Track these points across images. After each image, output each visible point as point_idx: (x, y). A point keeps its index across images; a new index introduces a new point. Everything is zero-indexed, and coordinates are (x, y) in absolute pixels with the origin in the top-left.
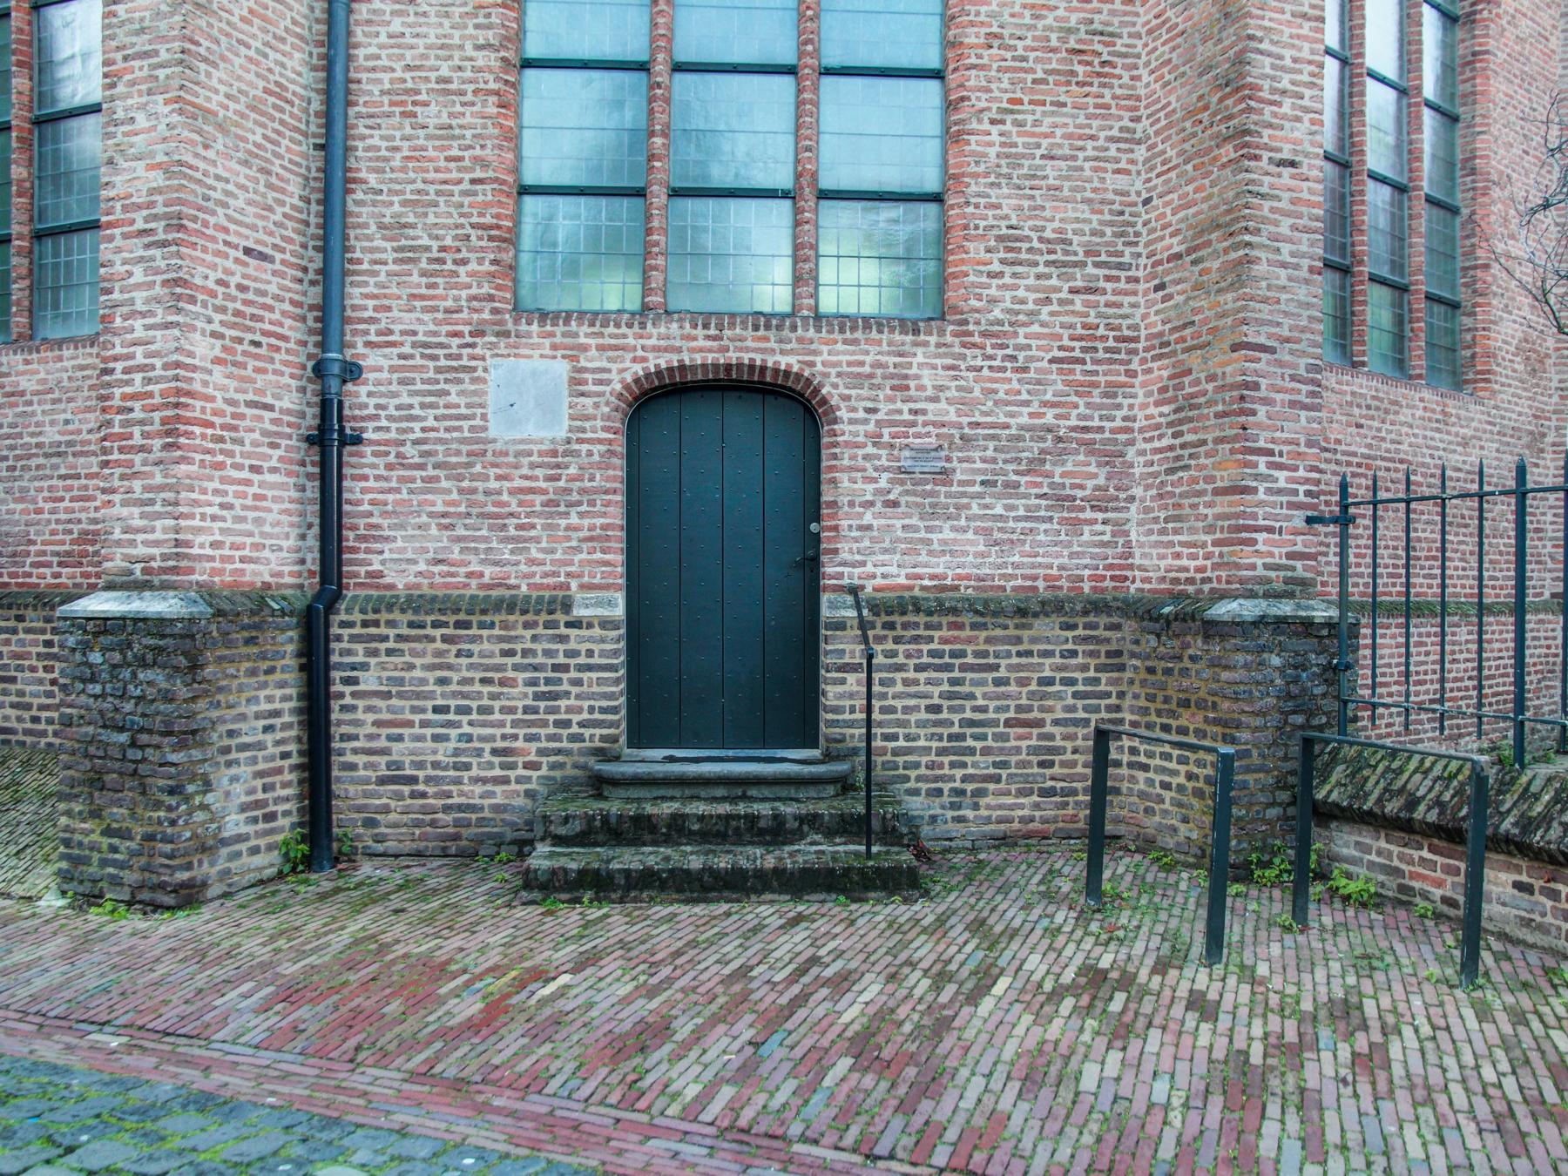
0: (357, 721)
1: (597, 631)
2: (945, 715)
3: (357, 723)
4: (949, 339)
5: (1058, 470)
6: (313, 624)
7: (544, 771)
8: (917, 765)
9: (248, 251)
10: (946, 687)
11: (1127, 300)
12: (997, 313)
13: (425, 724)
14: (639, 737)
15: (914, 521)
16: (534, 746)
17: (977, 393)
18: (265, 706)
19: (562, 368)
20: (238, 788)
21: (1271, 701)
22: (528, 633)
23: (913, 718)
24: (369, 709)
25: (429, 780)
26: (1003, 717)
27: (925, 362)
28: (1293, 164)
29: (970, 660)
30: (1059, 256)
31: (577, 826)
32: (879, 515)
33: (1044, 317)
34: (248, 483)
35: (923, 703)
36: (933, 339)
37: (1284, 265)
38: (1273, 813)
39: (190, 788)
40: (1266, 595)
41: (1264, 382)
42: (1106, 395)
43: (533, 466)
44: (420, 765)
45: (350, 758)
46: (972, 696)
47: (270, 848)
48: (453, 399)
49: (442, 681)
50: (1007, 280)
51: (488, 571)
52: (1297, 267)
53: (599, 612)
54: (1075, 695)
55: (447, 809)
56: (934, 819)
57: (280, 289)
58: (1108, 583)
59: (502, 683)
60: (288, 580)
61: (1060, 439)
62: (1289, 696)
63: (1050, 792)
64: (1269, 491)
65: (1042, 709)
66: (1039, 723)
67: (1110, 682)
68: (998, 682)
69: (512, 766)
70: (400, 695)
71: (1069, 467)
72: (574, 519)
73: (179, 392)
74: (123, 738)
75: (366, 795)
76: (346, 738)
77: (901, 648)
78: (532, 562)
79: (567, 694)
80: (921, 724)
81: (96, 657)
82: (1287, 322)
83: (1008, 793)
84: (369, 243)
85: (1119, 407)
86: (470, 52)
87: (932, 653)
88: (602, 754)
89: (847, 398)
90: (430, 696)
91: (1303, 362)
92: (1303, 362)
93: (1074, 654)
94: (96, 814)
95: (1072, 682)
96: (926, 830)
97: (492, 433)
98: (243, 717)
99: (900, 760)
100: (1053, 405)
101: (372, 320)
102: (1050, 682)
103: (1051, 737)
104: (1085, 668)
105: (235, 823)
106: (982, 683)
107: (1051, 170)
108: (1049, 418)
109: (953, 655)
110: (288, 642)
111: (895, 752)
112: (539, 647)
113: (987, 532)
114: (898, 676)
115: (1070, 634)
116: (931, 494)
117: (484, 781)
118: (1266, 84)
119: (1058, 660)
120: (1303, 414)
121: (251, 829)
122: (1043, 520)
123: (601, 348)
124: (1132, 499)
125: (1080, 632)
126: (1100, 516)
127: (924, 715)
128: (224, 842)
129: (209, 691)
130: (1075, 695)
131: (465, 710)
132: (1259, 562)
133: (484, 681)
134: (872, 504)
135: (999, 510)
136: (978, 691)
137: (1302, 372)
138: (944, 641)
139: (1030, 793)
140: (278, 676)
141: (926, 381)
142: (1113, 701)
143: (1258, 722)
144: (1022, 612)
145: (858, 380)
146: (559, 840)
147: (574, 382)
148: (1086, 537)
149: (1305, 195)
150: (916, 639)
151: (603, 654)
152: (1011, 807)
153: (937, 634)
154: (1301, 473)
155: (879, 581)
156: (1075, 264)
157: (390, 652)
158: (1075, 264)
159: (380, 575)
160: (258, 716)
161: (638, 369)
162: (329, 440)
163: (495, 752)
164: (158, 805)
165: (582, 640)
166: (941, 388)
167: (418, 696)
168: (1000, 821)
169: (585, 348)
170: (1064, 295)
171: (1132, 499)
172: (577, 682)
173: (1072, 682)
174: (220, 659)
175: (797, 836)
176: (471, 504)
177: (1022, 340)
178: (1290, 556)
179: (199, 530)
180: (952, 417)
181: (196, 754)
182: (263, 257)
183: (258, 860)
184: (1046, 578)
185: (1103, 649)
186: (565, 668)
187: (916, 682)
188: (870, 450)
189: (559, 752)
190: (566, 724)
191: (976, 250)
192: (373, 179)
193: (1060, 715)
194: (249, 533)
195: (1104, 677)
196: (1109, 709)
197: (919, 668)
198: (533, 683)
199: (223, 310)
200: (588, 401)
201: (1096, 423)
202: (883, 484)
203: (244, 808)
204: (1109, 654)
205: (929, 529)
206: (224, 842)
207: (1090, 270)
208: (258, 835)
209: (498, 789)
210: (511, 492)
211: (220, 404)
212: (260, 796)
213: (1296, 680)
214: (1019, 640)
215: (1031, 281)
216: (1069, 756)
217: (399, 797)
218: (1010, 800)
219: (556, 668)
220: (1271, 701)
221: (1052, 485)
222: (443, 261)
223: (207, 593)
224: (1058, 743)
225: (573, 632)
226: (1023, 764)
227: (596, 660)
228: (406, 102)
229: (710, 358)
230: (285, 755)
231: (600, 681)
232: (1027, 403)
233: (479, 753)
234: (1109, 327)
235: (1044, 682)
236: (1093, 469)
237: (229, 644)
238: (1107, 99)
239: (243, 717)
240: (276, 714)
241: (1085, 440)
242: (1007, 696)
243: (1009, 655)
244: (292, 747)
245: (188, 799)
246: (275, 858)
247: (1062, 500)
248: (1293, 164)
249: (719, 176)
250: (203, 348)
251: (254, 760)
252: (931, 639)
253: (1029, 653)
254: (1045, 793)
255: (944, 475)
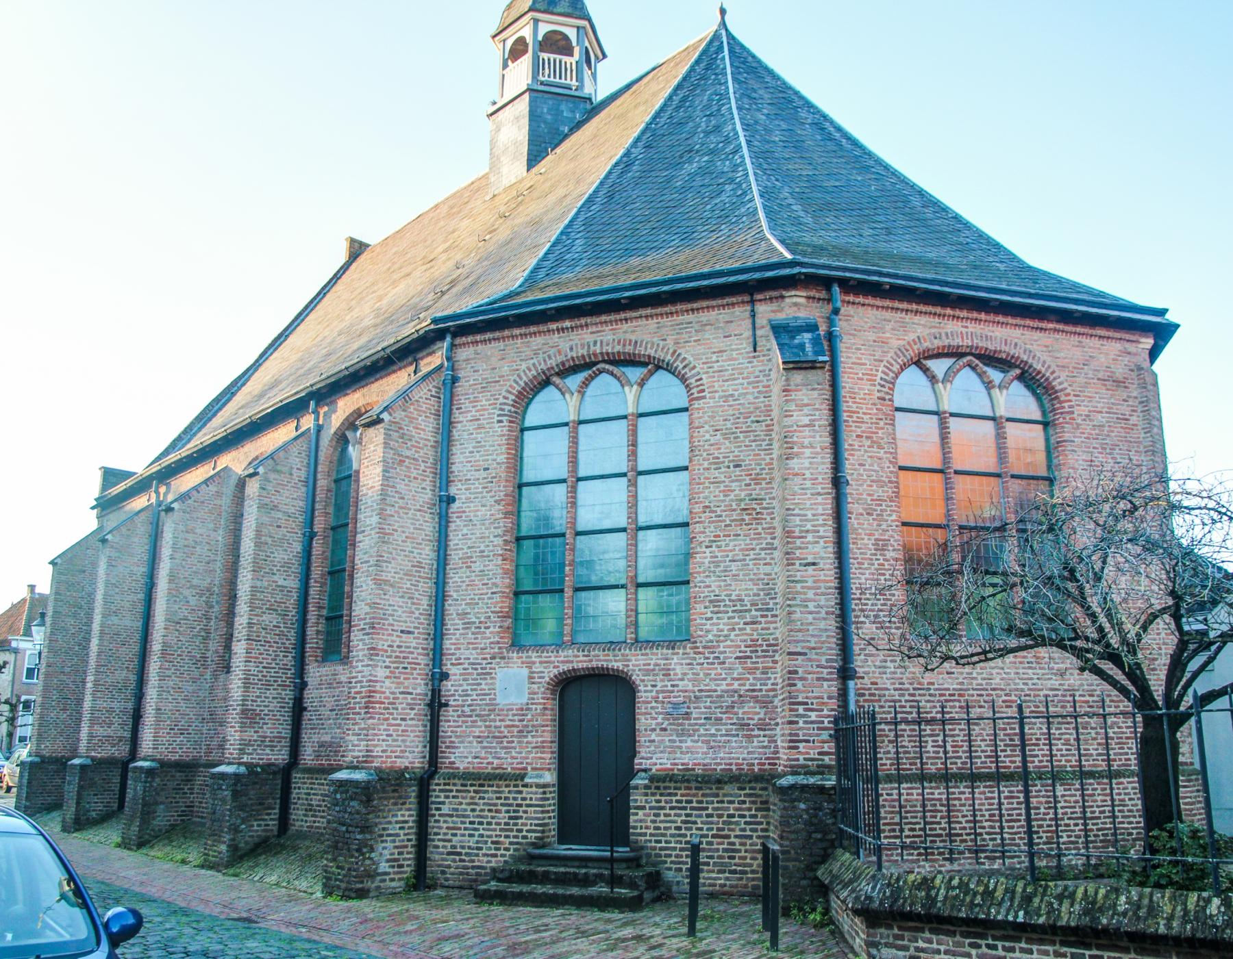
0: (440, 826)
1: (534, 789)
2: (683, 831)
3: (440, 828)
4: (688, 650)
5: (741, 711)
6: (424, 782)
7: (511, 852)
8: (670, 856)
9: (402, 632)
10: (683, 818)
11: (772, 626)
12: (710, 637)
13: (466, 829)
14: (562, 839)
15: (674, 737)
16: (508, 841)
17: (701, 675)
18: (400, 818)
19: (525, 672)
20: (386, 852)
21: (801, 826)
22: (507, 790)
23: (669, 832)
24: (445, 822)
25: (466, 854)
26: (710, 833)
27: (677, 661)
28: (814, 564)
29: (695, 805)
30: (739, 608)
31: (506, 874)
32: (658, 735)
33: (732, 637)
34: (400, 725)
35: (673, 825)
36: (681, 651)
37: (811, 613)
38: (804, 882)
39: (365, 850)
40: (805, 774)
41: (800, 670)
42: (763, 673)
43: (514, 715)
44: (463, 847)
45: (436, 843)
46: (695, 823)
47: (400, 879)
48: (483, 686)
49: (473, 810)
50: (715, 621)
51: (496, 761)
52: (818, 613)
53: (535, 780)
54: (746, 823)
55: (473, 867)
56: (678, 883)
57: (417, 645)
58: (767, 767)
59: (497, 811)
60: (417, 765)
61: (740, 696)
62: (812, 824)
63: (735, 872)
64: (805, 722)
65: (729, 830)
66: (728, 837)
67: (763, 817)
68: (708, 816)
69: (499, 849)
70: (457, 816)
71: (746, 709)
72: (530, 739)
73: (370, 691)
74: (344, 829)
75: (443, 860)
76: (436, 834)
77: (663, 798)
78: (513, 758)
79: (521, 818)
80: (672, 835)
81: (338, 796)
82: (813, 640)
83: (713, 871)
84: (453, 622)
85: (769, 679)
86: (492, 538)
87: (677, 801)
88: (534, 845)
89: (643, 681)
90: (468, 816)
91: (824, 658)
92: (824, 658)
93: (744, 802)
94: (334, 860)
95: (744, 816)
96: (675, 888)
97: (498, 701)
98: (390, 823)
99: (663, 853)
100: (738, 679)
101: (453, 654)
102: (732, 816)
103: (734, 844)
104: (750, 809)
105: (384, 867)
106: (700, 816)
107: (734, 566)
108: (736, 686)
109: (687, 802)
110: (413, 792)
111: (661, 849)
112: (511, 796)
113: (708, 742)
114: (662, 812)
115: (742, 792)
116: (681, 724)
117: (487, 855)
118: (797, 529)
119: (736, 805)
120: (825, 683)
121: (391, 870)
122: (734, 736)
123: (541, 662)
124: (777, 724)
125: (747, 791)
126: (762, 733)
127: (673, 831)
128: (379, 874)
129: (376, 810)
130: (746, 823)
131: (481, 823)
132: (801, 757)
133: (490, 811)
134: (654, 730)
135: (713, 731)
136: (699, 820)
137: (824, 663)
138: (682, 795)
139: (724, 872)
140: (407, 806)
141: (678, 671)
142: (764, 826)
143: (793, 836)
144: (719, 781)
145: (648, 672)
146: (499, 880)
147: (530, 678)
148: (755, 744)
149: (822, 578)
150: (670, 795)
151: (537, 799)
152: (715, 879)
153: (679, 792)
154: (825, 712)
155: (658, 766)
156: (746, 611)
157: (454, 797)
158: (746, 611)
159: (454, 763)
160: (397, 822)
161: (556, 671)
162: (436, 705)
163: (493, 843)
164: (352, 856)
165: (528, 793)
166: (685, 674)
167: (464, 816)
168: (710, 885)
169: (534, 663)
170: (741, 626)
171: (777, 724)
172: (525, 812)
173: (744, 816)
174: (380, 798)
175: (594, 884)
176: (489, 732)
177: (722, 649)
178: (820, 754)
179: (376, 746)
180: (690, 687)
181: (368, 836)
182: (409, 632)
183: (393, 884)
184: (737, 764)
185: (759, 800)
186: (521, 805)
187: (669, 815)
188: (654, 704)
189: (517, 843)
190: (520, 831)
191: (700, 608)
192: (455, 595)
193: (738, 833)
194: (396, 744)
195: (759, 814)
196: (762, 830)
197: (672, 808)
198: (508, 812)
199: (390, 657)
200: (535, 686)
201: (758, 687)
202: (660, 720)
203: (388, 861)
204: (762, 803)
205: (681, 741)
206: (379, 874)
207: (753, 613)
208: (395, 873)
209: (493, 859)
210: (506, 726)
211: (388, 694)
212: (396, 856)
213: (816, 816)
214: (717, 795)
215: (726, 620)
216: (743, 854)
217: (454, 861)
218: (714, 875)
219: (518, 805)
220: (801, 826)
221: (738, 719)
222: (480, 627)
223: (379, 770)
224: (738, 847)
225: (525, 789)
226: (720, 857)
227: (534, 802)
228: (467, 561)
229: (585, 665)
230: (409, 840)
231: (535, 812)
232: (725, 679)
233: (486, 842)
234: (764, 640)
235: (730, 816)
236: (757, 710)
237: (385, 792)
238: (760, 530)
239: (390, 823)
240: (406, 822)
241: (753, 695)
242: (712, 823)
243: (713, 802)
244: (413, 837)
245: (363, 854)
246: (402, 883)
247: (743, 725)
248: (814, 564)
249: (594, 580)
250: (381, 673)
251: (394, 841)
252: (676, 795)
253: (722, 802)
254: (731, 872)
255: (687, 715)
